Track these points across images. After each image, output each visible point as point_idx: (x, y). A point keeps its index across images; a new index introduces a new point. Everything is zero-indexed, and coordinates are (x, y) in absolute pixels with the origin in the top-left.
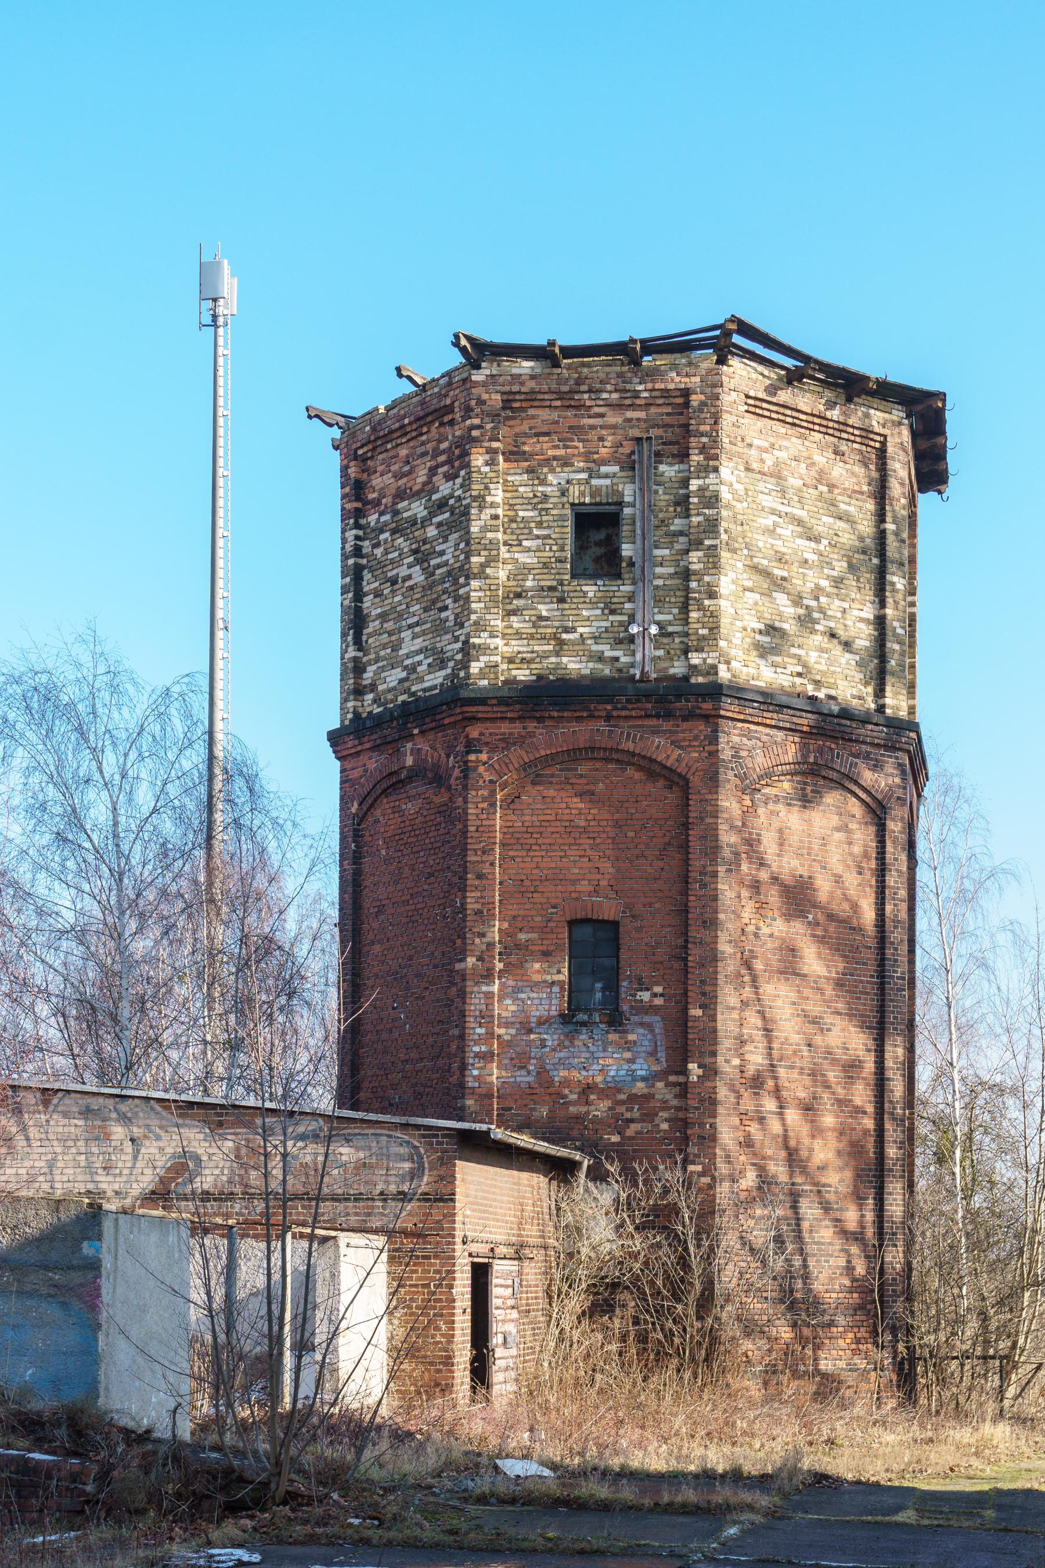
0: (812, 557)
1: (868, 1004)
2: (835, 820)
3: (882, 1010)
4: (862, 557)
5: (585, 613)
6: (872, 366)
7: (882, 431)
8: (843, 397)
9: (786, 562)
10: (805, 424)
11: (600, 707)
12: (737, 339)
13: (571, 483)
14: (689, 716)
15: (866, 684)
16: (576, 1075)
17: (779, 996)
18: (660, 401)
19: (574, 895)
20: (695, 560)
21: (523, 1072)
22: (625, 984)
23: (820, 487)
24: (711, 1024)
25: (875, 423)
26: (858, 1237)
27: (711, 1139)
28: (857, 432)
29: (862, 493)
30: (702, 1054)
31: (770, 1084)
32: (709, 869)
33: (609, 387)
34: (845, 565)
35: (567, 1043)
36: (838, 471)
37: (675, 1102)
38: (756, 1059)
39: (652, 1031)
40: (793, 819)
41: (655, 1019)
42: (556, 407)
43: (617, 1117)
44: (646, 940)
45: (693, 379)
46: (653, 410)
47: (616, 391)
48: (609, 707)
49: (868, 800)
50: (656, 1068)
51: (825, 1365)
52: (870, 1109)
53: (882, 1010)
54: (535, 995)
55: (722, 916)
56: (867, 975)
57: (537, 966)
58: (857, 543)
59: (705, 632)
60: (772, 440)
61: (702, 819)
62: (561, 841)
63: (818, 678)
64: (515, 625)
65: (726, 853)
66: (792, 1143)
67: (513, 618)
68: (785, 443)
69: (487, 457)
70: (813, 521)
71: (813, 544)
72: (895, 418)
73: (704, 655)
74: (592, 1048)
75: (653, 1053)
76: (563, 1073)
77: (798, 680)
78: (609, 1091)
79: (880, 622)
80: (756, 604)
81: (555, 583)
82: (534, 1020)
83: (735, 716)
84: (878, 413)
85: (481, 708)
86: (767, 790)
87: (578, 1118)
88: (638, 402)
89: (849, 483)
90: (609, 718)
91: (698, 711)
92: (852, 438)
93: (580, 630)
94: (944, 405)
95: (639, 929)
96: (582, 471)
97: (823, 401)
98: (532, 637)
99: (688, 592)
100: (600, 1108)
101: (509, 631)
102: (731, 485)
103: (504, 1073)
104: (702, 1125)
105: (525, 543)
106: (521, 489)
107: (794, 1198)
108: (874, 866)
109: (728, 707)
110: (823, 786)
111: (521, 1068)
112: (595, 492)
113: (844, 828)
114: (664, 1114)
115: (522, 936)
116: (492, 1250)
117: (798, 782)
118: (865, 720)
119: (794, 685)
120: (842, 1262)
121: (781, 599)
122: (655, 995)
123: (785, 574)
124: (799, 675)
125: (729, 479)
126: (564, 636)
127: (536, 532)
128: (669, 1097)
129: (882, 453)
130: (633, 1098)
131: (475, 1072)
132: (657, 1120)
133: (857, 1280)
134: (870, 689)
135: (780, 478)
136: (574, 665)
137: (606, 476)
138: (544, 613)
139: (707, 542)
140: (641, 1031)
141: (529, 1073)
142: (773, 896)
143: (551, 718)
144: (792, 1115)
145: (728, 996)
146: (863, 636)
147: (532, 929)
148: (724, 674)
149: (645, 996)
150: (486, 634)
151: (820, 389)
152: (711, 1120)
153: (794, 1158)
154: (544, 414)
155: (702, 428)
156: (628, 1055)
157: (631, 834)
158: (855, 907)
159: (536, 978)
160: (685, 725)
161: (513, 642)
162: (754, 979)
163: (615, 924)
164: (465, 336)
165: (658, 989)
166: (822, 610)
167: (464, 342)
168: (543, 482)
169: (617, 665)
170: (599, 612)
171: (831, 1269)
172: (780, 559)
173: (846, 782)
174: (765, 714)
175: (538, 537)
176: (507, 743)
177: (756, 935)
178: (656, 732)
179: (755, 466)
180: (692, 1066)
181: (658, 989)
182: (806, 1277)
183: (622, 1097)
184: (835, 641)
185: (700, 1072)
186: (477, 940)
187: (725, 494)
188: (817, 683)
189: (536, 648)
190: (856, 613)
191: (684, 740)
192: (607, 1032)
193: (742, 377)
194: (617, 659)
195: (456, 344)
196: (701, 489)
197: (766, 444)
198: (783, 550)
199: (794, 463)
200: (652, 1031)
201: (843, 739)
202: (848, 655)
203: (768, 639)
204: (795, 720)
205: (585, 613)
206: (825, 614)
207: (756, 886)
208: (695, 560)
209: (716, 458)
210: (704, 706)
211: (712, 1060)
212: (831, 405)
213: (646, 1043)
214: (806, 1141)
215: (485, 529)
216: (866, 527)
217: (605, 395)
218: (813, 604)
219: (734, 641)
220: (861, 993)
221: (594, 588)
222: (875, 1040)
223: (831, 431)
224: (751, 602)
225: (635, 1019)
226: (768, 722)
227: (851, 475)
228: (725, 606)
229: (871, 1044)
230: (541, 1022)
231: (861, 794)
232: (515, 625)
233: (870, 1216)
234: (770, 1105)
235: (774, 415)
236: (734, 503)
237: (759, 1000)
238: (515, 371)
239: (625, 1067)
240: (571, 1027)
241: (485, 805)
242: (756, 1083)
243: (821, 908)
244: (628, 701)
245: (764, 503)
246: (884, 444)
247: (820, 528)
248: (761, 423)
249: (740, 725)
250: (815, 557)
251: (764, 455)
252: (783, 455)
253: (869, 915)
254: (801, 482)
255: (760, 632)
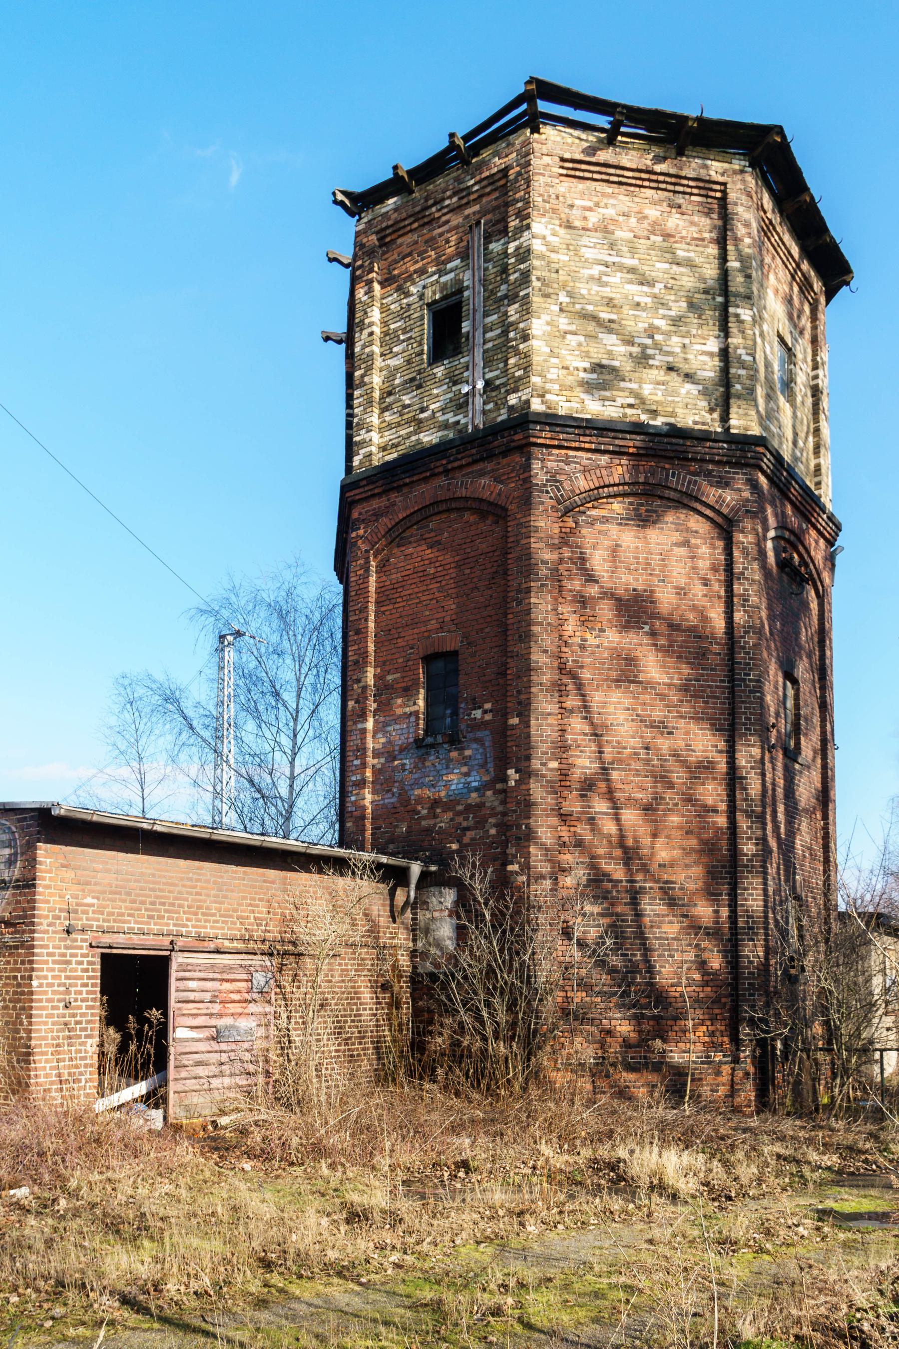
0: (644, 300)
1: (718, 706)
2: (676, 537)
3: (733, 713)
4: (703, 296)
5: (435, 391)
6: (687, 104)
7: (721, 179)
8: (674, 151)
9: (614, 306)
10: (633, 181)
11: (438, 464)
12: (543, 106)
13: (427, 287)
14: (507, 452)
15: (711, 410)
16: (428, 793)
17: (615, 706)
18: (488, 190)
19: (426, 634)
20: (512, 313)
21: (389, 795)
22: (462, 705)
23: (653, 238)
24: (525, 730)
25: (713, 173)
26: (713, 933)
27: (529, 836)
28: (691, 183)
29: (703, 240)
30: (519, 759)
31: (602, 786)
32: (524, 586)
33: (448, 193)
34: (684, 305)
35: (420, 765)
36: (674, 221)
37: (500, 809)
38: (584, 763)
39: (483, 745)
40: (628, 538)
41: (484, 734)
42: (416, 229)
43: (458, 826)
44: (478, 664)
45: (511, 157)
46: (484, 200)
47: (454, 194)
48: (444, 462)
49: (719, 520)
50: (486, 778)
51: (676, 1057)
52: (723, 807)
53: (733, 713)
54: (398, 727)
55: (536, 629)
56: (717, 681)
57: (399, 701)
58: (698, 285)
59: (521, 373)
60: (596, 199)
61: (518, 541)
62: (417, 590)
63: (654, 408)
64: (387, 419)
65: (543, 571)
66: (630, 842)
67: (387, 414)
68: (612, 201)
69: (366, 288)
70: (645, 268)
71: (645, 289)
72: (737, 167)
73: (520, 394)
74: (439, 767)
75: (484, 765)
76: (417, 792)
77: (629, 411)
78: (449, 805)
79: (725, 354)
80: (580, 345)
81: (414, 374)
82: (397, 748)
83: (548, 442)
84: (714, 163)
85: (357, 491)
86: (593, 512)
87: (428, 831)
88: (472, 197)
89: (693, 232)
90: (447, 472)
91: (512, 444)
92: (689, 190)
93: (432, 407)
94: (784, 137)
95: (473, 655)
96: (434, 274)
97: (651, 156)
98: (399, 424)
99: (508, 343)
100: (444, 821)
101: (384, 425)
102: (544, 238)
103: (376, 798)
104: (519, 827)
105: (395, 350)
106: (392, 307)
107: (635, 896)
108: (722, 578)
109: (538, 433)
110: (660, 506)
111: (388, 791)
112: (444, 287)
113: (686, 543)
114: (492, 820)
115: (390, 678)
116: (172, 943)
117: (630, 504)
118: (704, 437)
119: (625, 415)
120: (691, 956)
121: (610, 340)
122: (485, 712)
123: (614, 317)
124: (631, 406)
125: (542, 233)
126: (422, 416)
127: (402, 337)
128: (496, 803)
129: (723, 201)
130: (469, 808)
131: (353, 798)
132: (487, 826)
133: (709, 974)
134: (716, 415)
135: (607, 232)
136: (429, 438)
137: (451, 271)
138: (407, 402)
139: (522, 294)
140: (475, 746)
141: (393, 794)
142: (605, 611)
143: (406, 485)
144: (630, 816)
145: (544, 704)
146: (709, 368)
147: (396, 670)
148: (537, 405)
149: (477, 714)
150: (363, 431)
151: (647, 147)
152: (526, 821)
153: (630, 855)
154: (409, 239)
155: (517, 196)
156: (465, 769)
157: (467, 571)
158: (705, 619)
159: (399, 711)
160: (504, 461)
161: (386, 433)
162: (580, 687)
163: (455, 654)
164: (342, 192)
165: (488, 706)
166: (657, 346)
167: (340, 197)
168: (408, 294)
169: (459, 427)
170: (445, 387)
171: (678, 962)
172: (610, 303)
173: (687, 501)
174: (582, 439)
175: (403, 341)
176: (378, 514)
177: (583, 647)
178: (482, 474)
179: (577, 223)
180: (511, 772)
181: (488, 706)
182: (650, 969)
183: (460, 808)
184: (674, 374)
185: (517, 776)
186: (355, 686)
187: (537, 246)
188: (654, 413)
189: (402, 433)
190: (698, 347)
191: (504, 474)
192: (450, 751)
193: (554, 143)
194: (458, 422)
195: (336, 202)
196: (518, 248)
197: (591, 204)
198: (613, 295)
199: (621, 219)
200: (483, 745)
201: (679, 459)
202: (688, 386)
203: (595, 376)
204: (617, 442)
205: (435, 391)
206: (661, 350)
207: (583, 601)
208: (512, 313)
209: (528, 216)
210: (516, 437)
211: (526, 764)
212: (658, 159)
213: (479, 757)
214: (646, 841)
215: (364, 347)
216: (711, 271)
217: (447, 202)
218: (649, 341)
219: (549, 376)
220: (708, 697)
221: (442, 368)
222: (727, 741)
223: (663, 186)
224: (574, 343)
225: (471, 735)
226: (587, 446)
227: (691, 225)
228: (538, 346)
229: (722, 745)
230: (402, 750)
231: (708, 512)
232: (387, 419)
233: (725, 912)
234: (600, 806)
235: (596, 176)
236: (548, 254)
237: (585, 707)
238: (384, 210)
239: (463, 780)
240: (423, 751)
241: (362, 572)
242: (588, 786)
243: (664, 619)
244: (458, 453)
245: (587, 256)
246: (724, 192)
247: (653, 274)
248: (581, 186)
249: (556, 451)
250: (649, 300)
251: (588, 214)
252: (610, 212)
253: (719, 623)
254: (632, 235)
255: (585, 370)
